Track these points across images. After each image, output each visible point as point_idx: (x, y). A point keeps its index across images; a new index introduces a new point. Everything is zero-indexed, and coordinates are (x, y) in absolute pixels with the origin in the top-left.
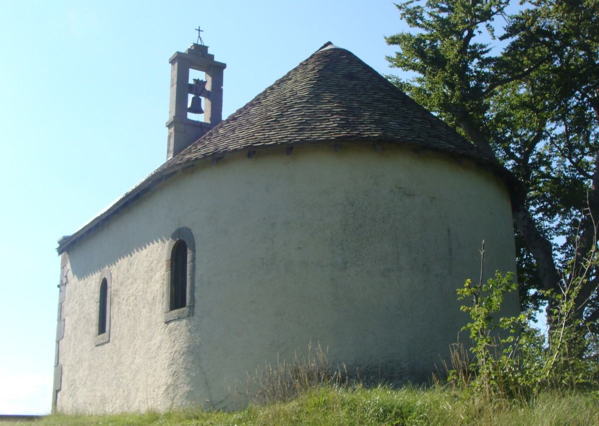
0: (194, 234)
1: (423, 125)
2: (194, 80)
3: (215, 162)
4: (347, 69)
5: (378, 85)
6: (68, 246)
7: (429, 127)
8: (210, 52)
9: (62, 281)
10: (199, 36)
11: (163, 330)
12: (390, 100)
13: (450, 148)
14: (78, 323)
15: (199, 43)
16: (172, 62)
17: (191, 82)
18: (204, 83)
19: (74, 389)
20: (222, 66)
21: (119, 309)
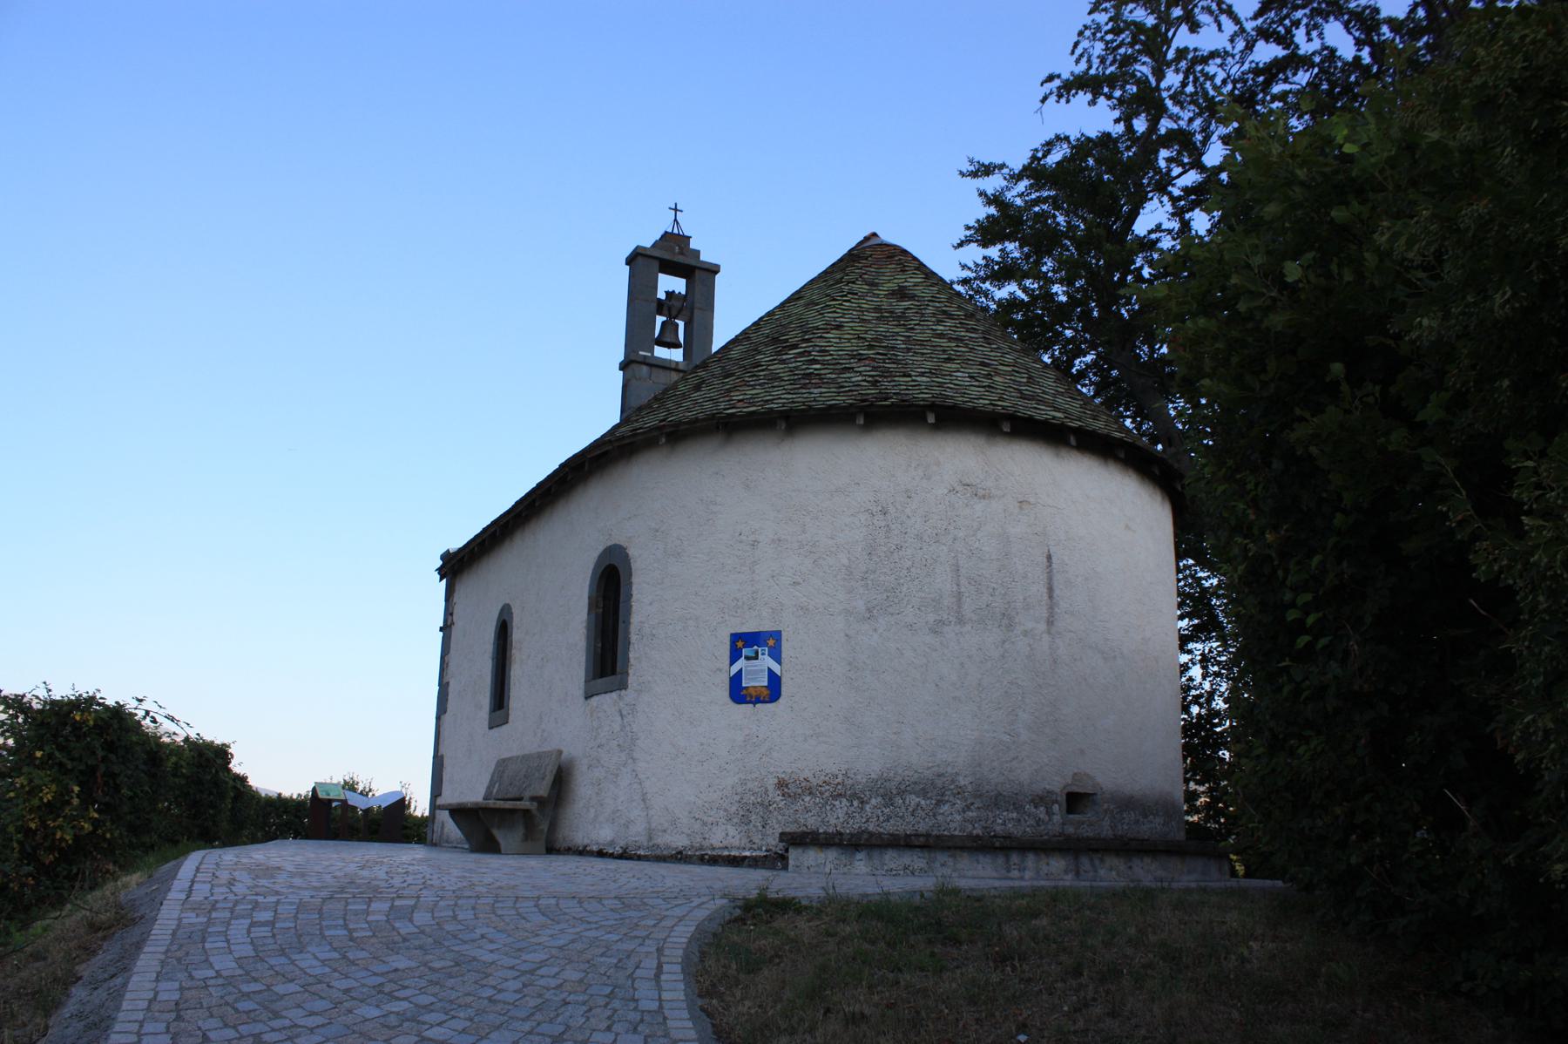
1: (1012, 378)
2: (667, 293)
4: (896, 281)
5: (944, 308)
6: (455, 566)
7: (1025, 380)
10: (675, 220)
12: (963, 334)
13: (1054, 418)
15: (676, 231)
20: (713, 270)
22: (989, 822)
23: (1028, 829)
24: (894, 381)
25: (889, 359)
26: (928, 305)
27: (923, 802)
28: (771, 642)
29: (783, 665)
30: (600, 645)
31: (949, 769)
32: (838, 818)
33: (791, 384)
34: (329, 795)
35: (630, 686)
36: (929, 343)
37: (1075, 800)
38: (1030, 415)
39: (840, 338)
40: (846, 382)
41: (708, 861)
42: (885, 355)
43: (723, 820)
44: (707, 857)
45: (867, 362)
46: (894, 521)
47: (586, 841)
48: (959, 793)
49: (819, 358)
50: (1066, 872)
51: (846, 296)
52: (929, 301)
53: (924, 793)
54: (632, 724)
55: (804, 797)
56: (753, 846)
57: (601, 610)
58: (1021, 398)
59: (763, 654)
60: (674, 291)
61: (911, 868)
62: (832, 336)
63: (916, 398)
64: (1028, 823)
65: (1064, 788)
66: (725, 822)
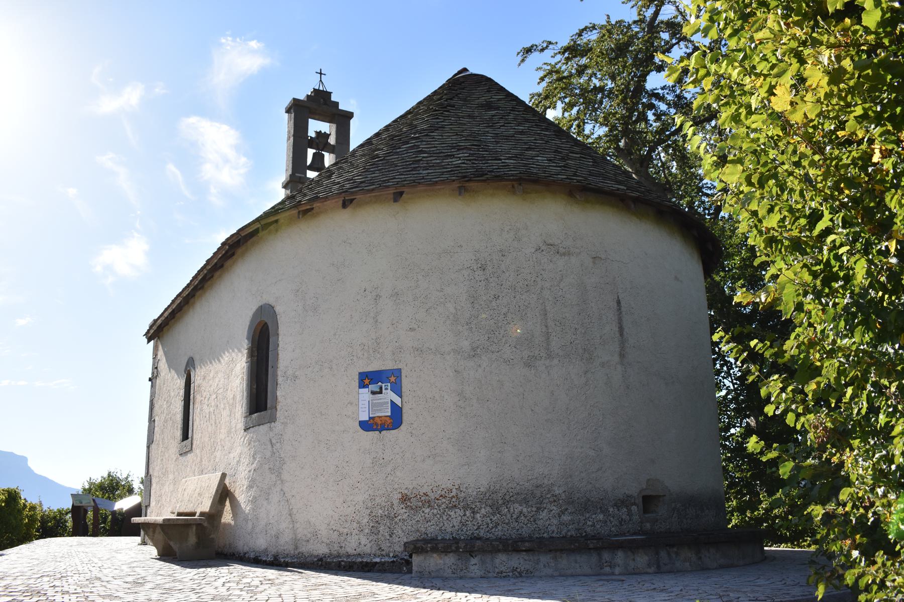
0: (277, 313)
2: (316, 132)
3: (301, 216)
4: (483, 98)
7: (591, 164)
8: (334, 98)
9: (153, 373)
10: (321, 80)
11: (242, 440)
13: (618, 189)
14: (165, 425)
15: (321, 88)
16: (288, 111)
17: (311, 134)
18: (327, 136)
19: (160, 507)
20: (349, 115)
21: (201, 410)
22: (581, 524)
23: (613, 529)
24: (487, 163)
25: (482, 148)
26: (510, 113)
27: (525, 510)
28: (393, 379)
29: (403, 398)
30: (255, 387)
31: (546, 481)
32: (454, 526)
33: (403, 168)
34: (81, 503)
35: (278, 419)
36: (513, 138)
37: (648, 501)
38: (600, 187)
39: (442, 136)
40: (449, 165)
41: (344, 567)
42: (479, 146)
43: (356, 531)
44: (343, 563)
45: (465, 151)
46: (492, 275)
47: (246, 549)
48: (555, 501)
49: (426, 149)
50: (649, 566)
51: (445, 107)
52: (511, 110)
53: (525, 501)
54: (280, 451)
55: (424, 509)
56: (382, 553)
57: (256, 358)
58: (589, 175)
59: (386, 389)
60: (320, 131)
61: (519, 570)
62: (436, 134)
63: (506, 174)
64: (613, 524)
65: (640, 492)
66: (358, 532)
